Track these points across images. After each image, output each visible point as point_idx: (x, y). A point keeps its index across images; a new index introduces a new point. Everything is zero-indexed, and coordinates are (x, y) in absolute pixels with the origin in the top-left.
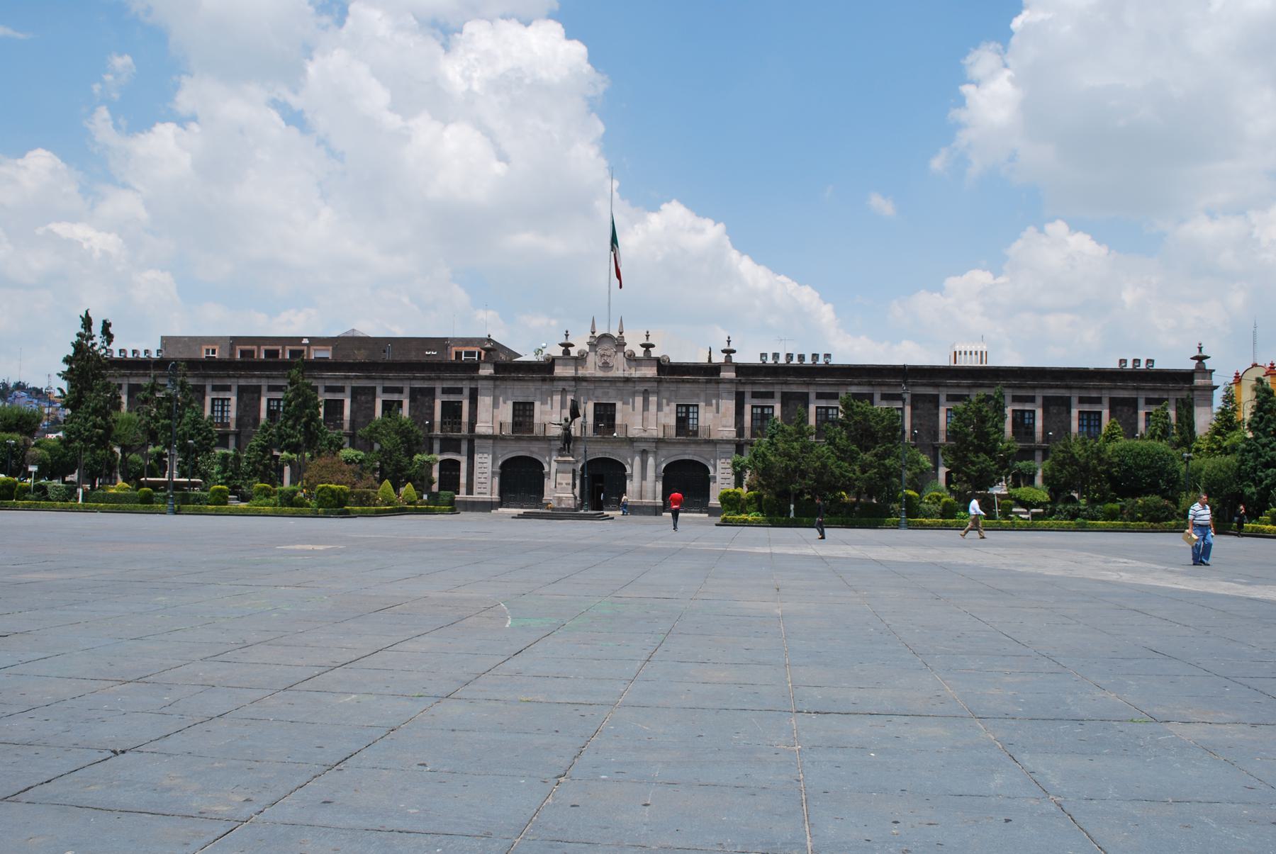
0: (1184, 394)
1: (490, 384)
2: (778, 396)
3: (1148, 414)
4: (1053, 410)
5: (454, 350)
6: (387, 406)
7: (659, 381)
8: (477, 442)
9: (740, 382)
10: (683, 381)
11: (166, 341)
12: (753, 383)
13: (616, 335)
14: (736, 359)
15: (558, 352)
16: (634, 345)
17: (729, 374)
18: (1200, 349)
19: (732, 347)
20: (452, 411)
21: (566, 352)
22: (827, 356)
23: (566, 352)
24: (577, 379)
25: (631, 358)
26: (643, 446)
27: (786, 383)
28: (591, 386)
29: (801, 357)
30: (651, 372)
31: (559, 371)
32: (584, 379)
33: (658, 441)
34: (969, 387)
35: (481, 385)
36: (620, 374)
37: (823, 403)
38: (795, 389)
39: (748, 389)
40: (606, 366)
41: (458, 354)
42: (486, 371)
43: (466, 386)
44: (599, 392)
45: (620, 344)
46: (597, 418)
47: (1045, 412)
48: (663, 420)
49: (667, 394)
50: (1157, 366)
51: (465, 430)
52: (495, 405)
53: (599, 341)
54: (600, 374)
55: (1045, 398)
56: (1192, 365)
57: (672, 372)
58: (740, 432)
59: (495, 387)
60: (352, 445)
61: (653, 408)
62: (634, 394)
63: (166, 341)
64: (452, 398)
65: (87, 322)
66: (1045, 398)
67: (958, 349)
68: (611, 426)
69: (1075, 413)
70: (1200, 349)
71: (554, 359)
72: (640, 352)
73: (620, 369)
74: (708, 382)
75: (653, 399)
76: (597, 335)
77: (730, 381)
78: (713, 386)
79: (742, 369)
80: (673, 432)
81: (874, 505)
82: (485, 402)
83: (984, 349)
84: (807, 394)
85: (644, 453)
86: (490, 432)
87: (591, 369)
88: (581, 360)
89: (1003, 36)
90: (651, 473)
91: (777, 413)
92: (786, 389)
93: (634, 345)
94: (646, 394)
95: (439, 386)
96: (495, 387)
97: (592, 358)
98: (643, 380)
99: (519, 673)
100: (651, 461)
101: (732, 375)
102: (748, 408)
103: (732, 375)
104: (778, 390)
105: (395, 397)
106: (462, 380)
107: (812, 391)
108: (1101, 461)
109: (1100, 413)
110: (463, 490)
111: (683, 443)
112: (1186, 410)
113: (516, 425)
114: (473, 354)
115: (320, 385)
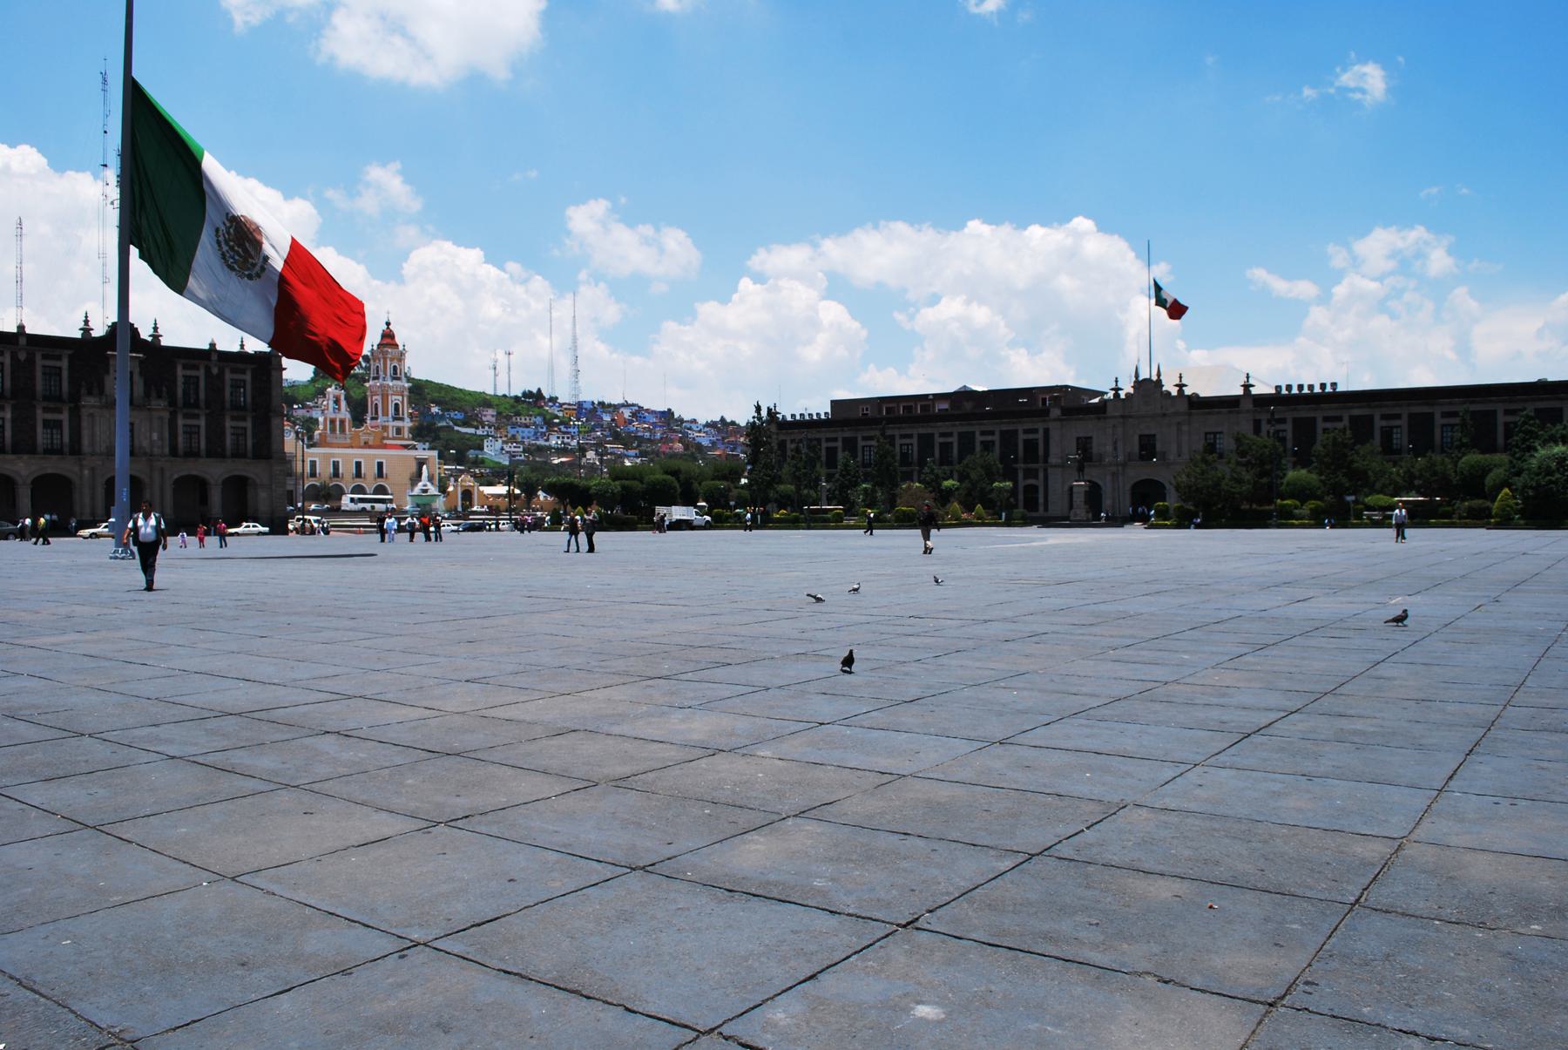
11: (834, 403)
13: (1154, 378)
14: (1254, 391)
17: (1248, 405)
29: (1289, 387)
38: (1303, 414)
42: (1055, 412)
43: (1041, 427)
46: (1142, 447)
58: (1046, 470)
63: (834, 403)
64: (1031, 436)
65: (758, 409)
72: (1174, 392)
75: (1185, 428)
95: (1020, 428)
99: (571, 495)
103: (1250, 406)
105: (989, 438)
108: (1435, 473)
110: (1041, 508)
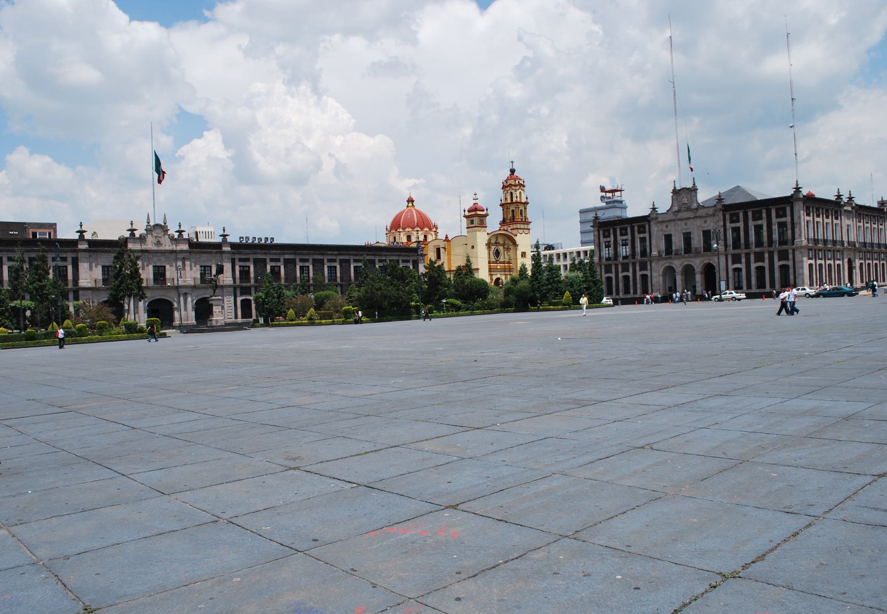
0: (415, 258)
1: (87, 254)
2: (252, 260)
3: (9, 268)
4: (344, 264)
5: (31, 231)
6: (302, 268)
7: (190, 252)
8: (81, 292)
9: (234, 253)
10: (204, 253)
12: (240, 253)
15: (127, 234)
16: (173, 231)
17: (227, 249)
18: (81, 226)
19: (226, 233)
20: (61, 273)
21: (132, 235)
22: (272, 239)
23: (132, 235)
24: (143, 251)
25: (172, 239)
26: (185, 290)
27: (256, 253)
28: (151, 256)
30: (185, 247)
31: (131, 246)
32: (146, 251)
33: (194, 287)
34: (336, 255)
35: (80, 255)
36: (167, 248)
37: (273, 264)
38: (260, 256)
39: (237, 257)
40: (159, 243)
41: (34, 234)
43: (70, 256)
44: (155, 259)
45: (163, 228)
47: (341, 266)
48: (194, 275)
49: (194, 260)
50: (275, 242)
51: (70, 285)
52: (91, 269)
53: (150, 230)
54: (155, 248)
55: (285, 259)
56: (76, 236)
57: (197, 247)
59: (90, 256)
60: (32, 299)
61: (188, 268)
62: (176, 260)
66: (285, 259)
67: (198, 230)
68: (164, 281)
69: (326, 266)
70: (81, 226)
71: (127, 238)
72: (176, 235)
73: (167, 246)
74: (217, 253)
75: (187, 263)
76: (152, 224)
77: (229, 252)
78: (219, 255)
79: (233, 245)
80: (199, 282)
81: (400, 311)
82: (83, 267)
83: (212, 230)
84: (265, 259)
85: (185, 294)
86: (89, 285)
87: (150, 245)
88: (142, 239)
89: (131, 20)
90: (190, 305)
91: (411, 267)
92: (255, 257)
93: (173, 231)
94: (184, 260)
96: (90, 256)
97: (150, 239)
98: (182, 251)
100: (189, 299)
101: (229, 249)
102: (237, 268)
103: (229, 249)
104: (251, 257)
106: (66, 252)
107: (268, 258)
109: (66, 267)
111: (204, 288)
112: (416, 264)
113: (156, 280)
114: (45, 234)
115: (268, 258)
